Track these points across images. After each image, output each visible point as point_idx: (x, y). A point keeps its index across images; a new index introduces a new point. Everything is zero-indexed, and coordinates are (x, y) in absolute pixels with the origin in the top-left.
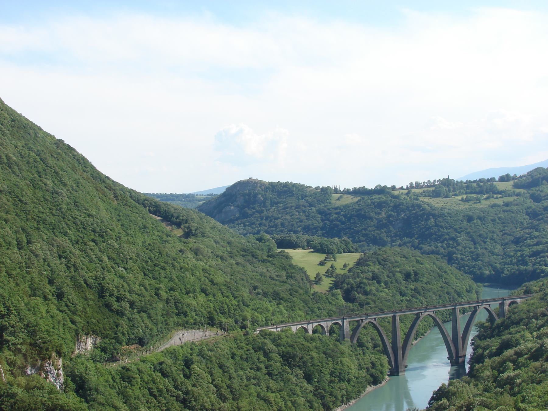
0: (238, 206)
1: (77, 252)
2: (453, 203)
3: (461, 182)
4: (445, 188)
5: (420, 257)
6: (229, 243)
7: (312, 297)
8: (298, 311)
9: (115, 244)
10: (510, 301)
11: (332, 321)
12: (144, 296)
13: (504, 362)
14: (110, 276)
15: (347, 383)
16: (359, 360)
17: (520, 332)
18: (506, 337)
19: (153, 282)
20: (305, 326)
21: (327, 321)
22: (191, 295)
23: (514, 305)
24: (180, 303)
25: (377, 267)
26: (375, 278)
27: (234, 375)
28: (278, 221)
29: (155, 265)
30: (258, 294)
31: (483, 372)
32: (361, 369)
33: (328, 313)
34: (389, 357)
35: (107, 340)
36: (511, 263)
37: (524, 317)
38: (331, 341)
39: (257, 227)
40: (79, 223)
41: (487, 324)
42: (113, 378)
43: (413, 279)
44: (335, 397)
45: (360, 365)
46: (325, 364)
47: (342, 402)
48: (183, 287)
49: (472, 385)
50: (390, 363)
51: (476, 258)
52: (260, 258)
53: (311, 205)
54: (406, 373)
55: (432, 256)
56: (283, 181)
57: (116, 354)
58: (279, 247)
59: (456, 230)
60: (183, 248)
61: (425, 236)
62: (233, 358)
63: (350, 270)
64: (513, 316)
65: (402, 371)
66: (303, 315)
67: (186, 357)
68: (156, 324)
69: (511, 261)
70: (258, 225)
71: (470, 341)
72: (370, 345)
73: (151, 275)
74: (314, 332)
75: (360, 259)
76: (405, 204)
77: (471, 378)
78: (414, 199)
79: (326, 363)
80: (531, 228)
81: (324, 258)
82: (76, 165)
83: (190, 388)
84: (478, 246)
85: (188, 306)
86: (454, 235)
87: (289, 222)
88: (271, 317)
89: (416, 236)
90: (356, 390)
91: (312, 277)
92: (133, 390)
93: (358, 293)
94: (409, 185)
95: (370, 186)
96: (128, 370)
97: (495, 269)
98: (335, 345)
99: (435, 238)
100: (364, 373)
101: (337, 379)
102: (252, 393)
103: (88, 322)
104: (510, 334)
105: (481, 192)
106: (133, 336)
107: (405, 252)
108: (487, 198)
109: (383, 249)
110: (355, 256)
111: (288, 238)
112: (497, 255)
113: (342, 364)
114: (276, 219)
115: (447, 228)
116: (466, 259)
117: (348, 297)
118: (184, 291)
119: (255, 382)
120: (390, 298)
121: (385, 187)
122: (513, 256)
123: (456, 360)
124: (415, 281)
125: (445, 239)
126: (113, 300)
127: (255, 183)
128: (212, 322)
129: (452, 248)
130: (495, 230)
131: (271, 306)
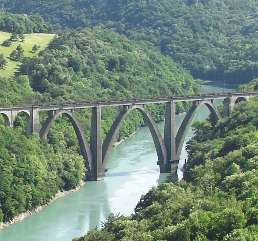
5: (128, 42)
10: (236, 97)
11: (18, 110)
13: (230, 163)
15: (33, 185)
16: (49, 159)
17: (248, 132)
18: (232, 137)
21: (12, 110)
23: (242, 102)
25: (75, 51)
26: (72, 64)
31: (203, 175)
32: (51, 169)
33: (12, 102)
34: (85, 157)
36: (238, 57)
38: (16, 135)
41: (207, 124)
43: (118, 68)
44: (19, 200)
45: (50, 164)
47: (27, 208)
49: (189, 189)
54: (106, 179)
55: (143, 42)
59: (172, 14)
63: (41, 54)
64: (240, 115)
69: (238, 55)
71: (185, 144)
72: (63, 143)
75: (55, 41)
77: (188, 181)
79: (10, 160)
81: (9, 38)
86: (169, 21)
89: (123, 19)
93: (50, 81)
97: (217, 63)
98: (21, 138)
99: (146, 23)
100: (54, 175)
101: (21, 180)
104: (237, 134)
107: (109, 35)
109: (83, 31)
110: (50, 37)
112: (221, 47)
113: (29, 163)
115: (161, 12)
116: (183, 50)
117: (37, 85)
120: (89, 89)
122: (240, 49)
123: (166, 165)
124: (121, 71)
125: (159, 25)
129: (167, 35)
130: (220, 16)
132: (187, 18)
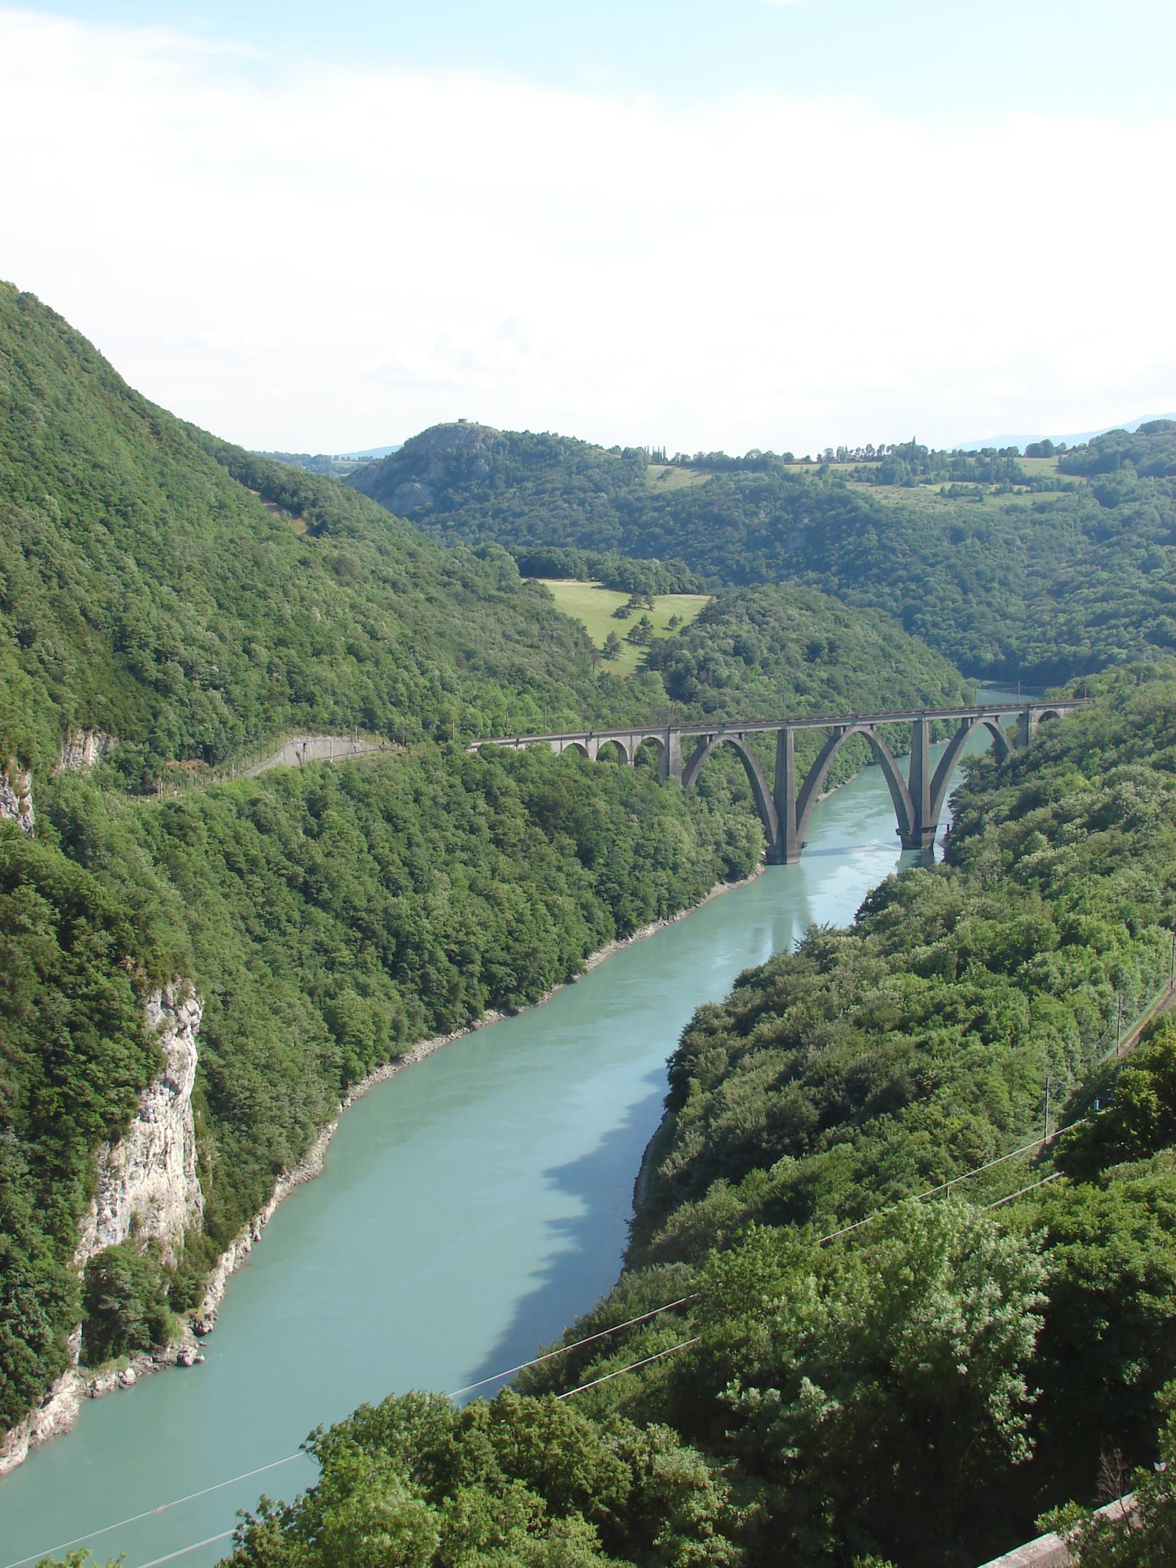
0: (430, 483)
1: (67, 546)
2: (925, 498)
3: (942, 452)
4: (905, 466)
6: (411, 555)
7: (597, 684)
8: (566, 711)
9: (154, 534)
10: (1041, 712)
12: (217, 654)
13: (1028, 832)
14: (142, 604)
15: (670, 872)
17: (1063, 775)
19: (240, 623)
20: (582, 742)
21: (631, 734)
22: (325, 658)
23: (1052, 720)
24: (300, 673)
25: (746, 627)
26: (741, 651)
27: (419, 838)
28: (522, 522)
29: (243, 588)
30: (475, 668)
31: (979, 853)
34: (765, 821)
35: (131, 745)
37: (1072, 745)
38: (639, 780)
39: (473, 532)
40: (71, 481)
41: (987, 761)
42: (146, 824)
43: (826, 658)
46: (623, 829)
47: (659, 913)
48: (306, 639)
50: (767, 835)
51: (966, 624)
52: (481, 591)
53: (598, 488)
54: (804, 862)
55: (870, 610)
56: (536, 430)
57: (151, 777)
58: (522, 575)
59: (924, 559)
60: (307, 555)
61: (856, 570)
62: (416, 801)
63: (684, 632)
64: (1049, 744)
65: (793, 856)
66: (578, 720)
67: (311, 792)
68: (244, 717)
69: (1044, 634)
70: (474, 527)
72: (725, 795)
73: (234, 609)
74: (602, 757)
76: (813, 494)
77: (953, 865)
78: (834, 485)
80: (1091, 564)
82: (66, 353)
83: (319, 859)
84: (971, 596)
85: (318, 681)
87: (546, 525)
88: (505, 718)
90: (691, 888)
91: (599, 642)
92: (189, 855)
93: (702, 682)
94: (823, 455)
95: (736, 451)
96: (179, 810)
98: (648, 786)
99: (877, 576)
100: (708, 854)
101: (648, 862)
102: (457, 880)
103: (89, 702)
104: (1042, 778)
105: (984, 478)
106: (192, 741)
108: (998, 493)
110: (699, 602)
111: (545, 555)
112: (1014, 620)
113: (662, 831)
114: (517, 515)
116: (944, 625)
117: (678, 689)
118: (309, 649)
119: (465, 856)
121: (769, 455)
123: (913, 835)
124: (831, 662)
125: (900, 579)
126: (147, 657)
127: (472, 431)
128: (371, 721)
131: (506, 698)
132: (951, 567)
